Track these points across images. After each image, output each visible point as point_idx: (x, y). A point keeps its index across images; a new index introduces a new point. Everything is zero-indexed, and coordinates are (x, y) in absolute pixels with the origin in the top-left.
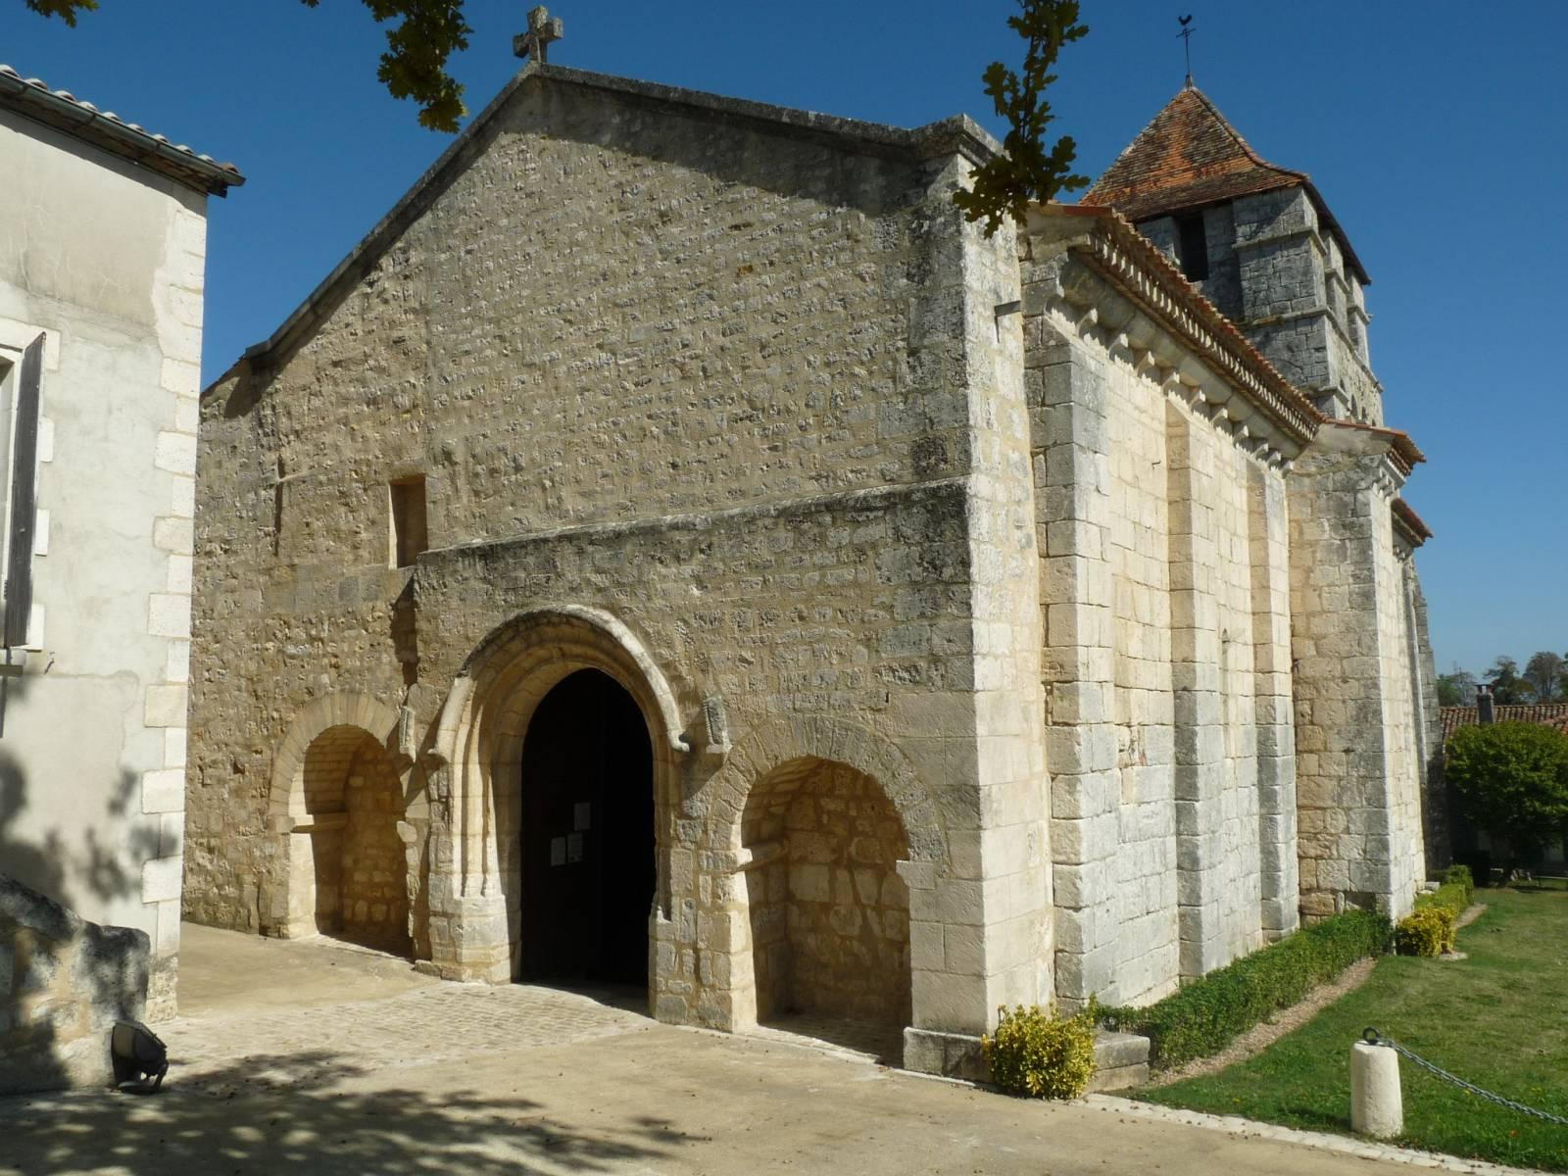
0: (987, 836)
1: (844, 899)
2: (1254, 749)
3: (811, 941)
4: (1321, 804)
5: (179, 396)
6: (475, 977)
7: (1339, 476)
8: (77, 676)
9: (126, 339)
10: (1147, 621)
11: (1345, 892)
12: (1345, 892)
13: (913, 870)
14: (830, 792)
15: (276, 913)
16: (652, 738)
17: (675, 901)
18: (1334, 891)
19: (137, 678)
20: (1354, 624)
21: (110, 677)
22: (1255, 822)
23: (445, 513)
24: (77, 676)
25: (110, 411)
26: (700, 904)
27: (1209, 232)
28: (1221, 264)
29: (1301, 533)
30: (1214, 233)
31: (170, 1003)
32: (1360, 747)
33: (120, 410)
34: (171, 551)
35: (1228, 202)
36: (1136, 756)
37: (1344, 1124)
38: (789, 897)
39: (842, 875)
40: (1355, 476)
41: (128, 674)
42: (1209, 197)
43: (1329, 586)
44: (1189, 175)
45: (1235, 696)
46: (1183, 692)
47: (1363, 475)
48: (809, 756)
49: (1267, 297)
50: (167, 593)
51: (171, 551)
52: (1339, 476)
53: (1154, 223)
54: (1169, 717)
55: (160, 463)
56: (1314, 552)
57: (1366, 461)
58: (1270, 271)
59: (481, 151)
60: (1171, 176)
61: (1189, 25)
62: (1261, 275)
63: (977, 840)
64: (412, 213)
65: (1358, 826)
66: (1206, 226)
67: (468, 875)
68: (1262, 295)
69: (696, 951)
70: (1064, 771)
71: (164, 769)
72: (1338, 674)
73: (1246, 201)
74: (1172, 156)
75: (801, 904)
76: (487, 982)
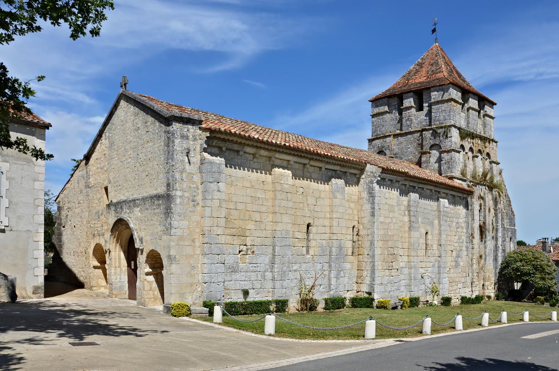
4: (362, 269)
5: (39, 173)
6: (116, 297)
7: (369, 179)
8: (17, 231)
9: (25, 163)
10: (258, 220)
11: (366, 292)
12: (366, 292)
18: (363, 292)
19: (31, 231)
20: (370, 220)
21: (24, 231)
24: (17, 231)
25: (22, 178)
27: (424, 97)
29: (361, 195)
30: (425, 97)
31: (42, 295)
33: (25, 177)
34: (39, 206)
37: (262, 332)
40: (373, 179)
41: (29, 230)
42: (423, 87)
43: (366, 210)
44: (425, 78)
47: (374, 179)
50: (38, 214)
51: (39, 206)
52: (369, 179)
53: (408, 94)
55: (35, 188)
56: (363, 200)
57: (376, 175)
58: (440, 110)
59: (116, 110)
60: (420, 78)
62: (438, 112)
64: (107, 124)
65: (369, 275)
68: (437, 118)
71: (39, 250)
72: (367, 234)
73: (435, 88)
74: (423, 71)
76: (118, 298)
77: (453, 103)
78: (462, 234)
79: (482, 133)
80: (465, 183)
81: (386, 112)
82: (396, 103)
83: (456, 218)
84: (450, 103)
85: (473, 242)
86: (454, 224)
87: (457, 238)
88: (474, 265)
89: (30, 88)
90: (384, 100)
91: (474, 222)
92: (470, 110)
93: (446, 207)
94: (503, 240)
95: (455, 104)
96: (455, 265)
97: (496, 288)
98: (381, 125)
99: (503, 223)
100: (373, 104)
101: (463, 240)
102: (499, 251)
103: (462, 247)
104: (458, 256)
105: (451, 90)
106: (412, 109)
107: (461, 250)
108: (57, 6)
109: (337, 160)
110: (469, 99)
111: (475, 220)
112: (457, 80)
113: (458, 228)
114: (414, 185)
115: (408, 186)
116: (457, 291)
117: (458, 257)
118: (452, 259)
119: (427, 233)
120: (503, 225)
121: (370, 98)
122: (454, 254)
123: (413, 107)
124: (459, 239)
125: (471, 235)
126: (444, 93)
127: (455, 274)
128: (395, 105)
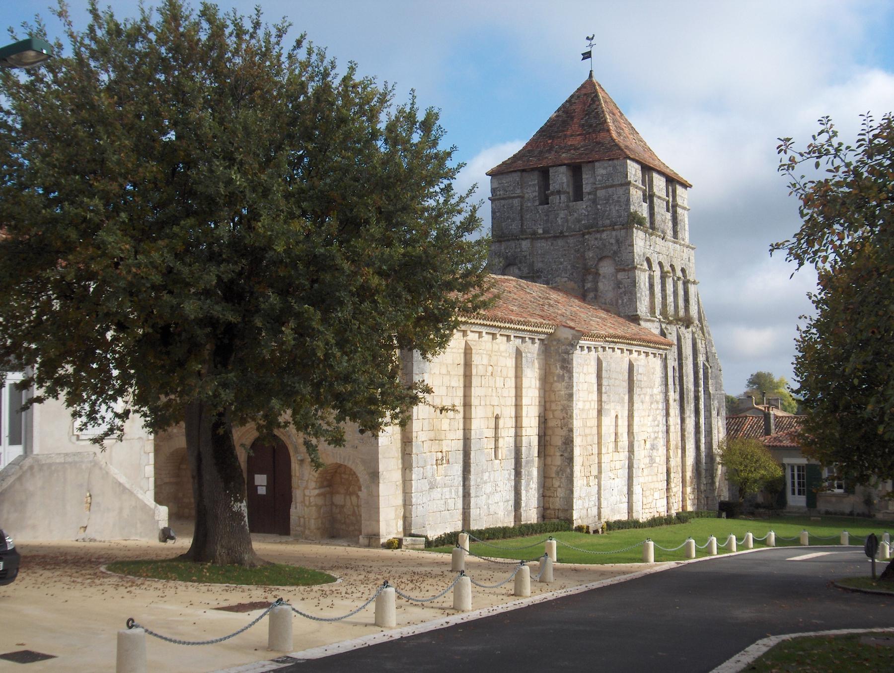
0: (381, 485)
1: (348, 504)
2: (513, 455)
3: (339, 516)
13: (363, 494)
14: (344, 473)
15: (468, 437)
16: (564, 594)
17: (298, 504)
22: (513, 483)
23: (434, 573)
26: (305, 505)
27: (584, 176)
28: (589, 194)
32: (566, 455)
35: (593, 162)
36: (444, 461)
38: (332, 504)
39: (348, 497)
45: (503, 437)
46: (467, 440)
48: (337, 463)
49: (609, 215)
54: (461, 448)
61: (593, 42)
63: (378, 486)
66: (583, 173)
67: (636, 390)
69: (305, 519)
70: (407, 466)
75: (336, 506)
78: (658, 412)
82: (536, 182)
86: (647, 398)
87: (650, 418)
89: (461, 222)
90: (514, 175)
98: (508, 218)
100: (494, 181)
101: (659, 421)
103: (658, 432)
104: (653, 447)
107: (656, 438)
108: (137, 391)
112: (576, 149)
113: (652, 403)
116: (653, 505)
118: (646, 453)
119: (617, 416)
121: (489, 169)
122: (648, 446)
124: (654, 421)
127: (650, 477)
128: (534, 185)
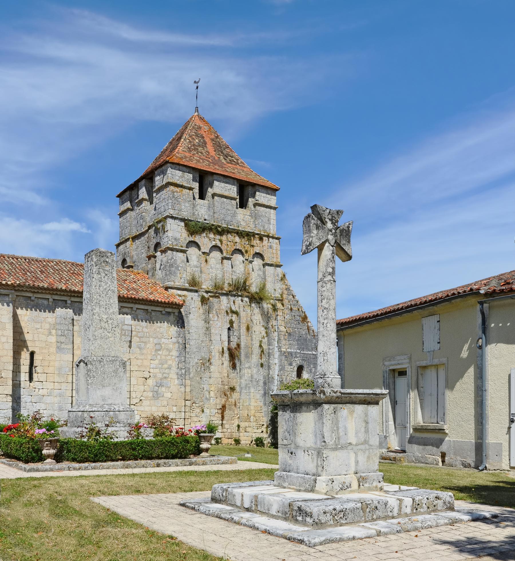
77: (172, 188)
79: (252, 226)
80: (196, 294)
81: (128, 210)
83: (155, 338)
84: (168, 189)
85: (210, 370)
88: (212, 399)
91: (212, 343)
92: (215, 197)
93: (126, 325)
94: (280, 369)
95: (176, 189)
96: (154, 397)
97: (269, 432)
99: (280, 345)
102: (274, 383)
105: (170, 171)
106: (144, 203)
109: (38, 288)
110: (213, 182)
111: (214, 342)
114: (160, 310)
115: (51, 300)
117: (158, 387)
120: (279, 348)
123: (145, 200)
125: (209, 361)
126: (164, 176)
